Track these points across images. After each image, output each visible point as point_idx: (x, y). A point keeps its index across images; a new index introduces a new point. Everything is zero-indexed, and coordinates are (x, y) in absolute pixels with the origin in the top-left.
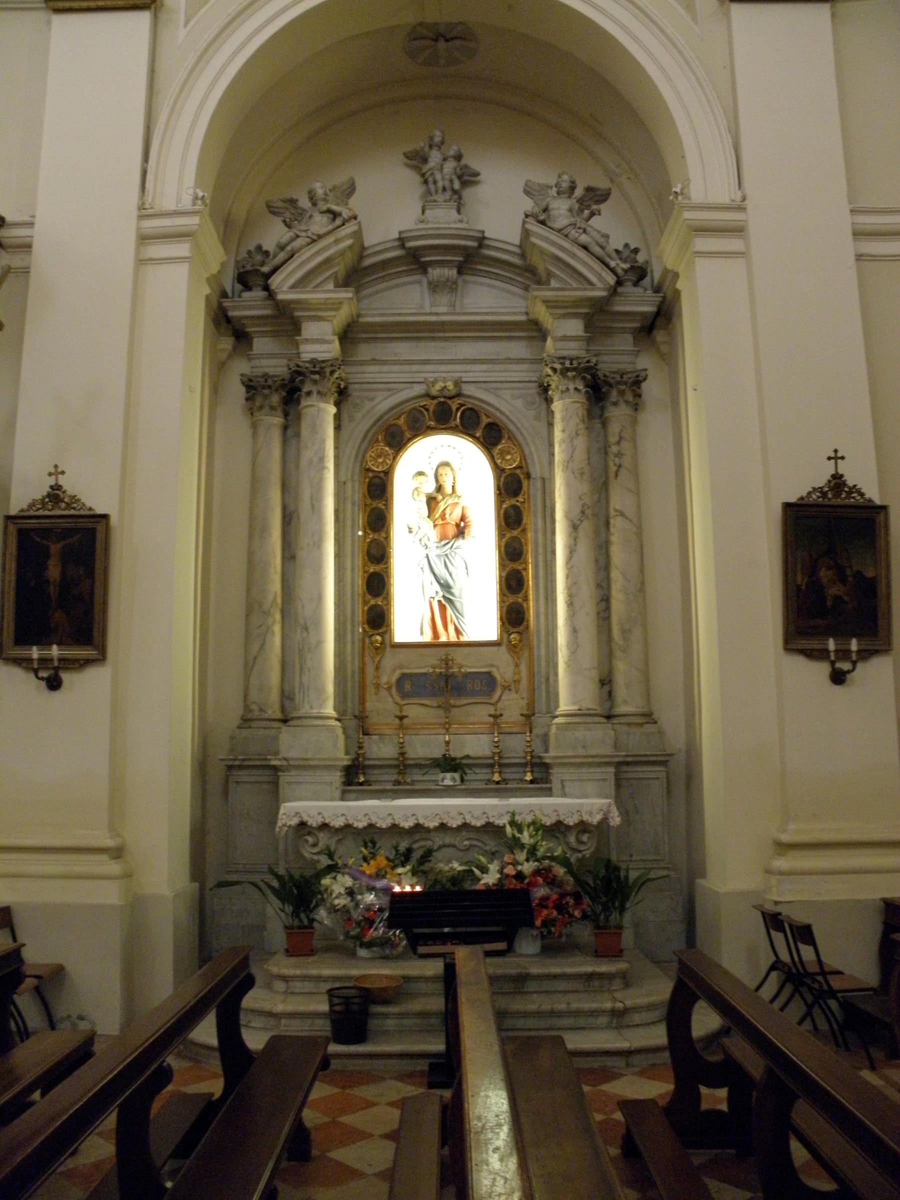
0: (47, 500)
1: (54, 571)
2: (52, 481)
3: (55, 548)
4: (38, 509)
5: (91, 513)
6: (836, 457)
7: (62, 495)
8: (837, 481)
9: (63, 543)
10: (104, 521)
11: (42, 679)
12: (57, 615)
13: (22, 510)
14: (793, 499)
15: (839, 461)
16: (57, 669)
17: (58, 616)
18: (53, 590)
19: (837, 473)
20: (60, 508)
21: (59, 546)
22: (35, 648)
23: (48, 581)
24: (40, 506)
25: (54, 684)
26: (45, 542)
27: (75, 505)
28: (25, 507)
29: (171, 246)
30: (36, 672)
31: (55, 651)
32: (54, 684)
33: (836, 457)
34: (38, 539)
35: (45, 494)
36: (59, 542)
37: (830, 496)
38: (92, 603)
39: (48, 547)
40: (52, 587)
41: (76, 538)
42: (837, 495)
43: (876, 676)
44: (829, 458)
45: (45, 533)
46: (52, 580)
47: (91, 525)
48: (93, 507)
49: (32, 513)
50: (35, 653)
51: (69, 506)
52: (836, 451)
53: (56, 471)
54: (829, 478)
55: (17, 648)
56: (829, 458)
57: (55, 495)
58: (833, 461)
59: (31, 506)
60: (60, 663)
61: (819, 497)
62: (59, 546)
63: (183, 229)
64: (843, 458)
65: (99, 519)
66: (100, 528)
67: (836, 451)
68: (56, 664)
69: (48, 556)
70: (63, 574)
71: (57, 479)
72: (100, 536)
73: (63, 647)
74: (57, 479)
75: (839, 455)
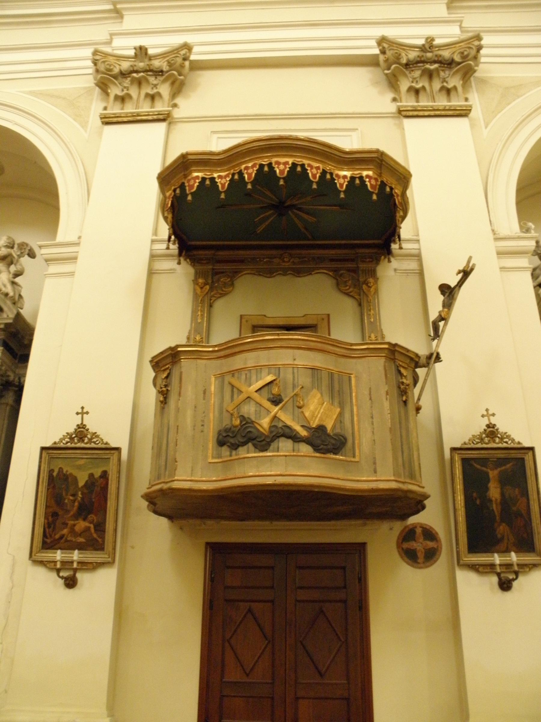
0: (74, 436)
1: (494, 492)
2: (485, 421)
3: (493, 474)
4: (478, 443)
5: (519, 446)
6: (83, 413)
7: (86, 432)
8: (491, 429)
9: (499, 469)
10: (530, 453)
11: (62, 578)
12: (501, 527)
13: (55, 443)
14: (48, 444)
15: (85, 415)
16: (75, 570)
17: (502, 529)
18: (495, 508)
19: (491, 423)
20: (494, 442)
21: (496, 472)
22: (59, 552)
23: (490, 501)
24: (68, 440)
25: (71, 583)
26: (484, 469)
27: (95, 440)
28: (467, 441)
29: (516, 260)
30: (58, 571)
31: (76, 555)
32: (71, 583)
33: (83, 413)
34: (478, 467)
35: (482, 430)
36: (496, 469)
37: (76, 441)
38: (530, 520)
39: (487, 474)
40: (494, 506)
41: (508, 466)
42: (81, 440)
43: (99, 585)
44: (78, 413)
45: (484, 461)
46: (494, 499)
47: (519, 456)
48: (521, 442)
49: (62, 445)
50: (59, 555)
51: (90, 441)
52: (83, 408)
53: (488, 413)
54: (75, 427)
55: (470, 555)
56: (78, 413)
57: (491, 431)
58: (80, 416)
59: (472, 440)
60: (78, 566)
61: (67, 443)
62: (496, 472)
63: (524, 249)
64: (87, 413)
65: (526, 451)
66: (528, 458)
67: (83, 408)
68: (58, 566)
69: (488, 481)
70: (502, 494)
71: (489, 420)
72: (529, 464)
73: (521, 554)
74: (489, 420)
75: (85, 411)
